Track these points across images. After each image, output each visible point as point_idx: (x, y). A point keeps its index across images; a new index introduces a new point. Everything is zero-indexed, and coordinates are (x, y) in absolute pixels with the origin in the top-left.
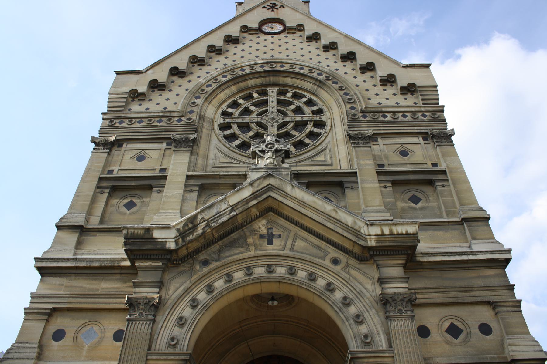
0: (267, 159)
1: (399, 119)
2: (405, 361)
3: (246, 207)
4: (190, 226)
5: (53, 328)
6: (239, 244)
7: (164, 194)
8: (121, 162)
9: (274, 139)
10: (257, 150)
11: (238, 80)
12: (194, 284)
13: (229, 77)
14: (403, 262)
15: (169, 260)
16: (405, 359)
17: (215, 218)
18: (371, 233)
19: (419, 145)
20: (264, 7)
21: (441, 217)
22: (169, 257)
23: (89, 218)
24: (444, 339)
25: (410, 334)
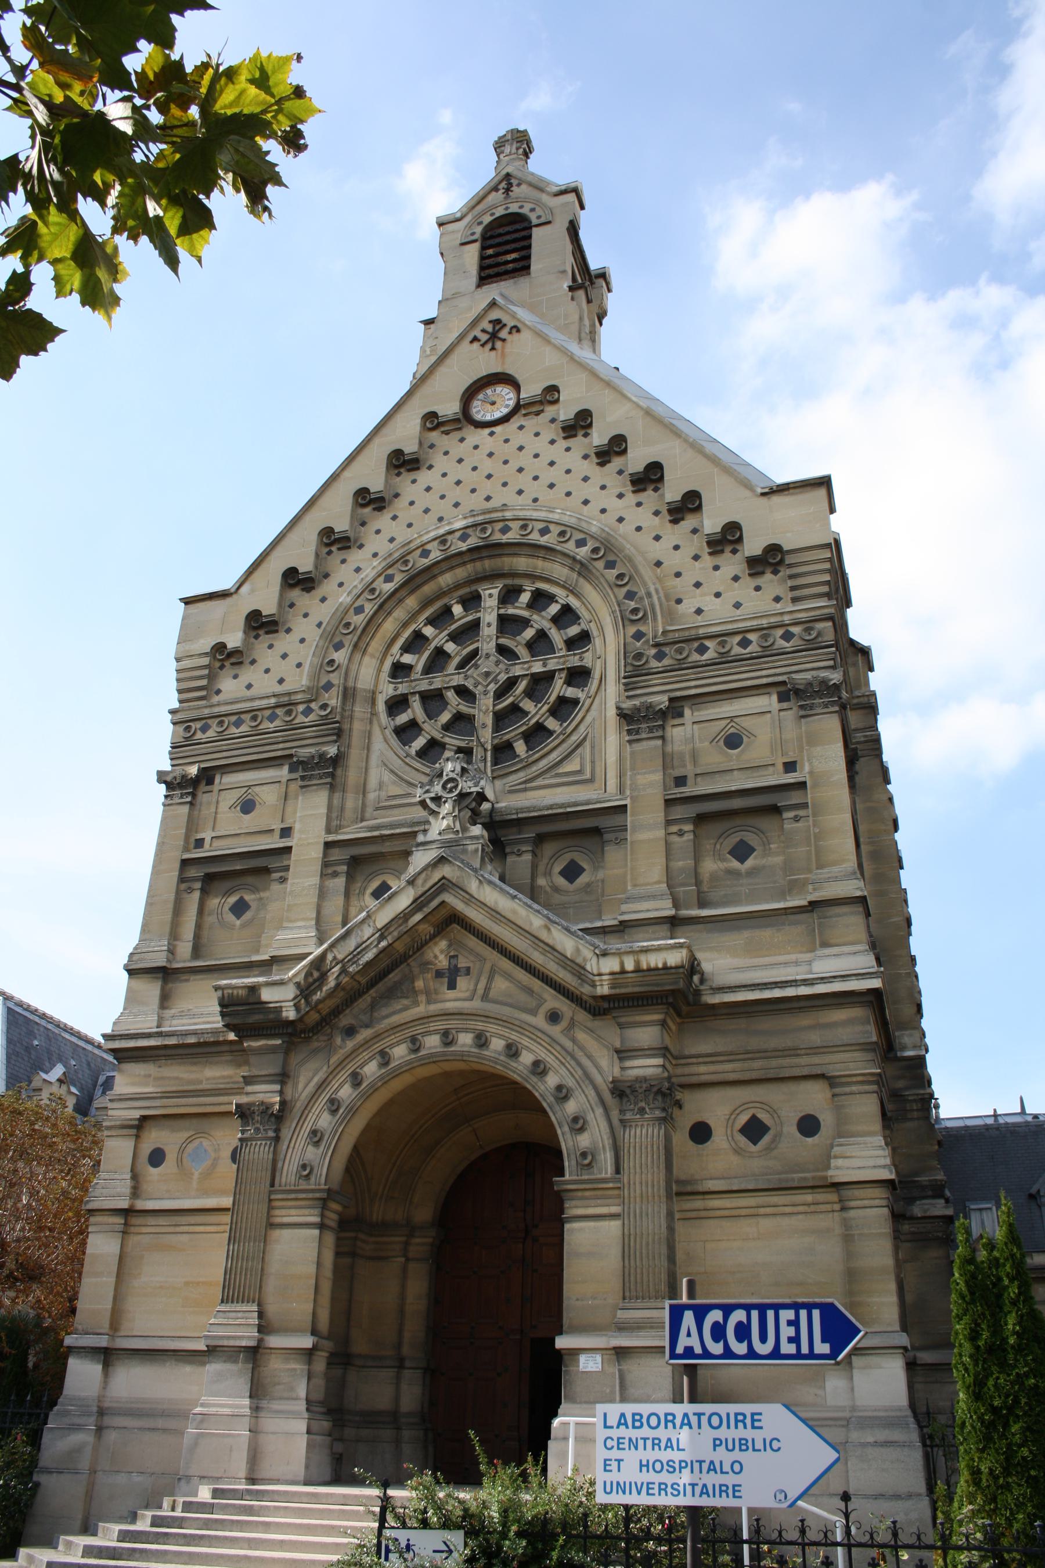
0: (443, 818)
1: (733, 653)
3: (404, 928)
4: (316, 974)
5: (146, 1148)
8: (215, 818)
9: (458, 769)
11: (419, 581)
12: (332, 1074)
13: (399, 578)
15: (291, 1035)
17: (355, 956)
19: (769, 715)
20: (475, 339)
23: (175, 946)
24: (733, 1144)
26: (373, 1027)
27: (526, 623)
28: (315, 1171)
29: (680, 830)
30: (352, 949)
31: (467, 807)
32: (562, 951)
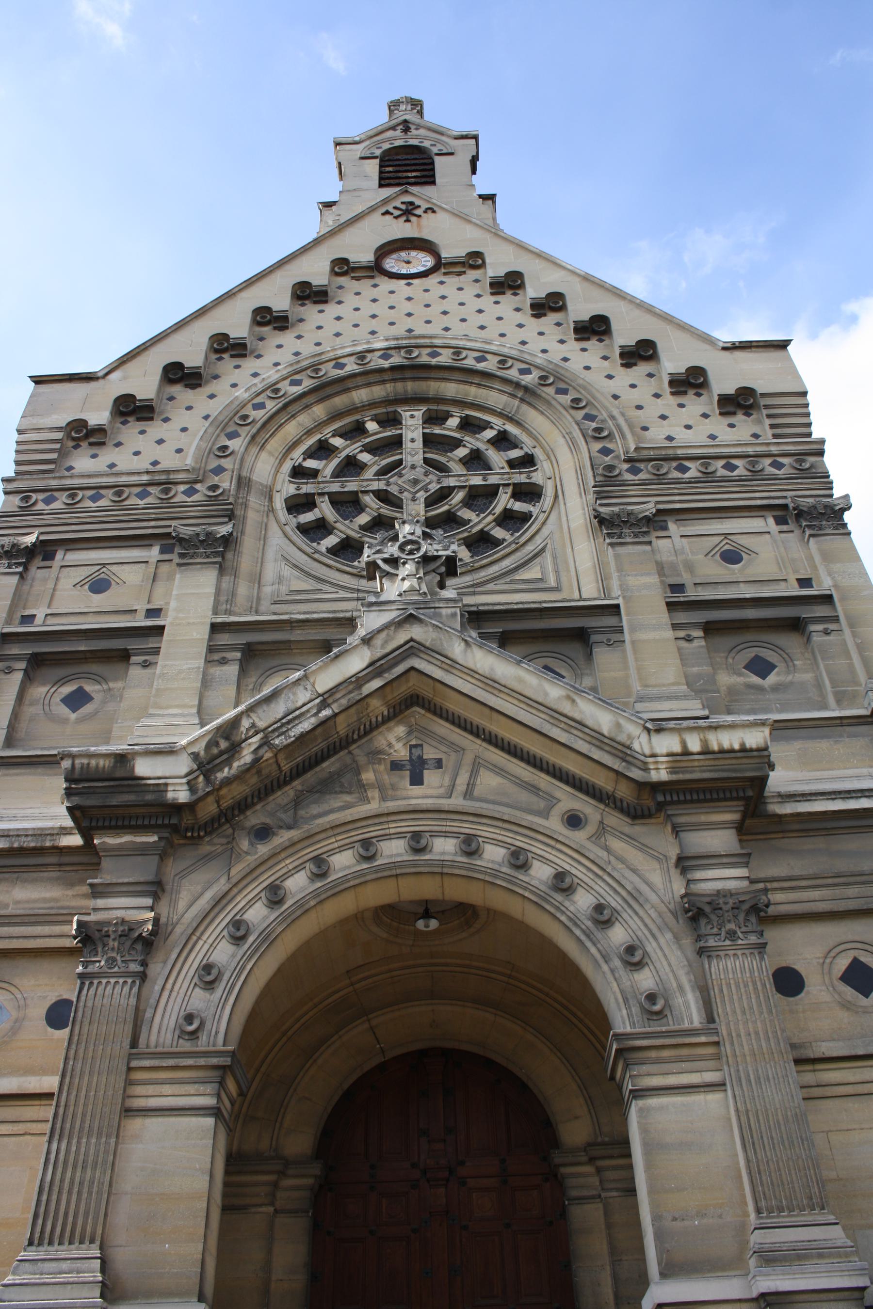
0: (403, 579)
1: (718, 474)
3: (355, 696)
4: (224, 744)
6: (342, 786)
7: (159, 669)
8: (52, 596)
9: (419, 531)
10: (378, 559)
11: (329, 390)
12: (239, 885)
13: (308, 383)
14: (735, 817)
16: (746, 1048)
17: (283, 725)
18: (658, 751)
19: (767, 536)
20: (387, 213)
21: (825, 707)
22: (174, 821)
24: (836, 996)
26: (298, 828)
27: (457, 443)
31: (434, 571)
32: (596, 728)
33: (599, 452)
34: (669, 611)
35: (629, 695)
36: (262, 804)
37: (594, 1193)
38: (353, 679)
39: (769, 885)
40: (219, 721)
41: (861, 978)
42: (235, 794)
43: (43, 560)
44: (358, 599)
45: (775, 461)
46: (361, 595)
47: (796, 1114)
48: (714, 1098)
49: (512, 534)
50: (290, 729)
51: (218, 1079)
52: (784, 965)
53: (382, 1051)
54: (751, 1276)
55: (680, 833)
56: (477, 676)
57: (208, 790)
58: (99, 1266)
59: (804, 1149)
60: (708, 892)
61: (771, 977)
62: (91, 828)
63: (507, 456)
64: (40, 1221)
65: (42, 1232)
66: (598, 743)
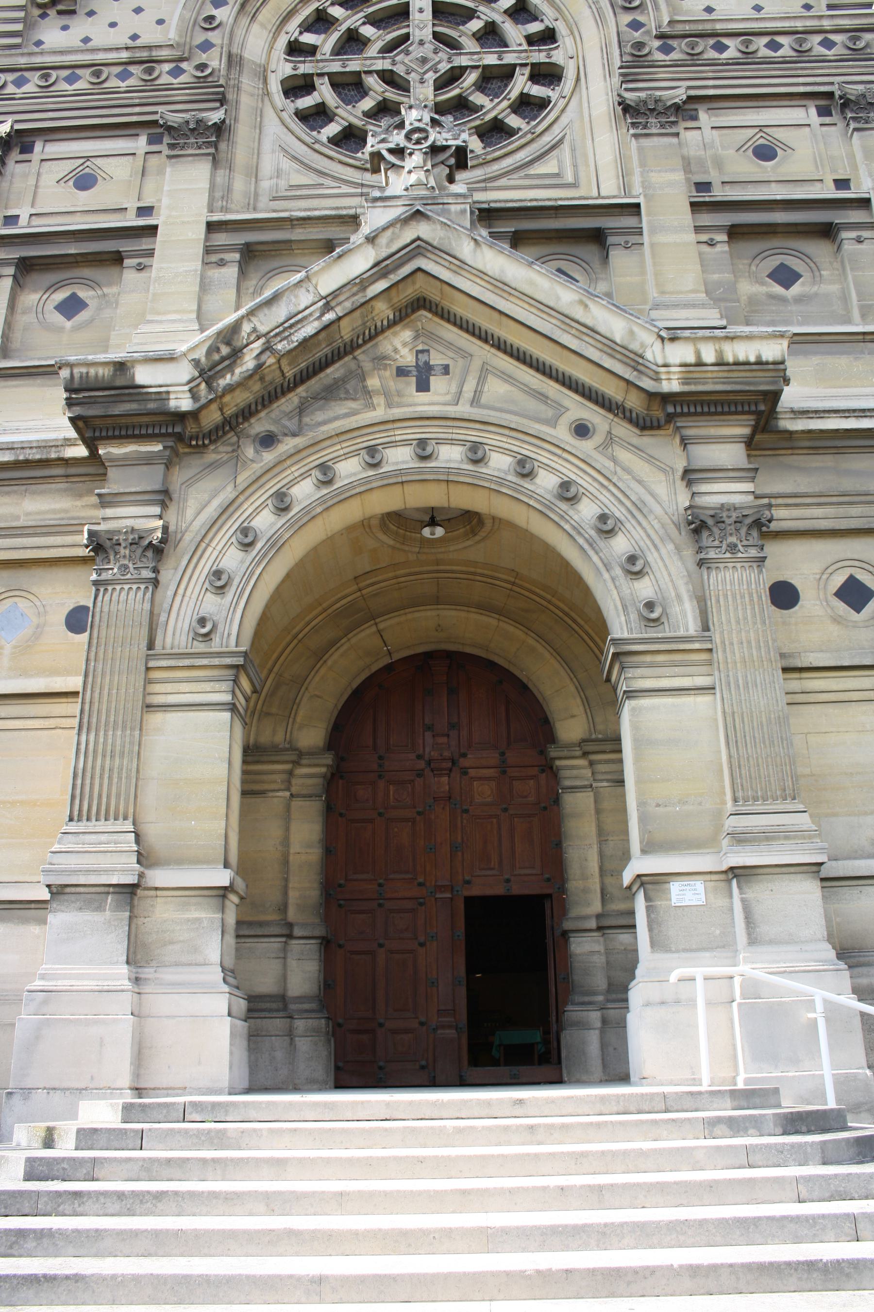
0: (410, 172)
1: (760, 54)
2: (738, 660)
3: (360, 299)
4: (225, 350)
6: (347, 392)
7: (154, 273)
8: (35, 193)
9: (427, 119)
10: (383, 148)
14: (747, 431)
15: (180, 438)
16: (737, 655)
17: (285, 329)
18: (671, 360)
19: (807, 129)
21: (849, 321)
22: (178, 429)
24: (829, 611)
25: (751, 600)
26: (304, 435)
28: (220, 627)
29: (712, 240)
30: (281, 320)
32: (608, 335)
33: (628, 26)
34: (693, 212)
35: (645, 302)
36: (266, 411)
37: (586, 783)
38: (357, 281)
39: (773, 501)
40: (219, 326)
41: (854, 594)
42: (239, 401)
43: (21, 153)
44: (362, 195)
45: (826, 38)
46: (365, 190)
47: (779, 717)
48: (703, 700)
49: (528, 123)
50: (293, 334)
51: (233, 678)
52: (782, 579)
53: (390, 653)
54: (722, 853)
55: (688, 446)
56: (486, 278)
57: (210, 397)
58: (133, 838)
59: (783, 748)
60: (712, 505)
61: (767, 590)
62: (95, 439)
63: (526, 30)
64: (77, 802)
65: (80, 811)
66: (609, 351)
